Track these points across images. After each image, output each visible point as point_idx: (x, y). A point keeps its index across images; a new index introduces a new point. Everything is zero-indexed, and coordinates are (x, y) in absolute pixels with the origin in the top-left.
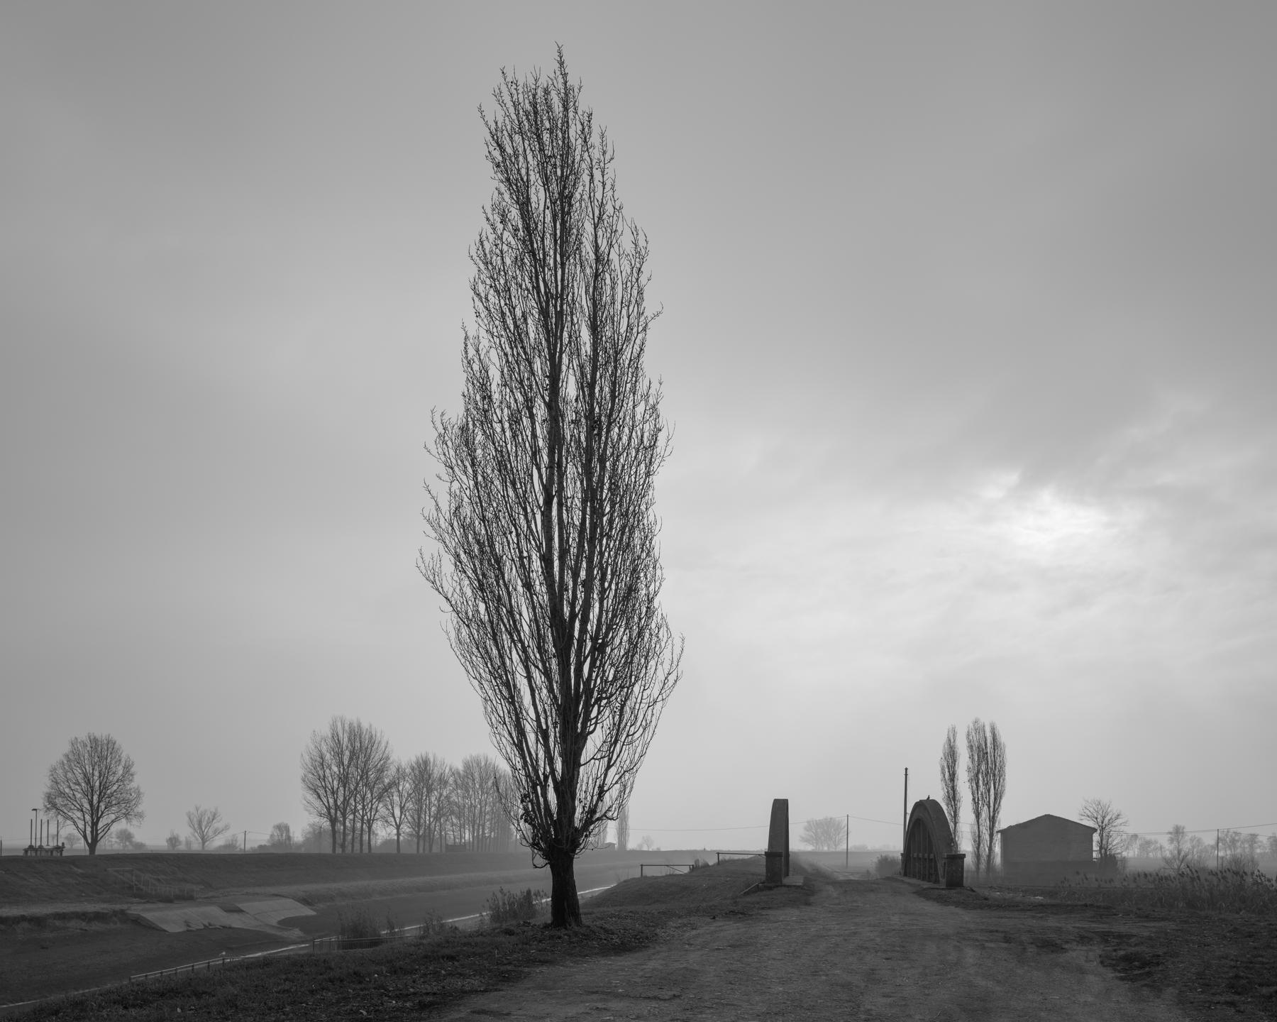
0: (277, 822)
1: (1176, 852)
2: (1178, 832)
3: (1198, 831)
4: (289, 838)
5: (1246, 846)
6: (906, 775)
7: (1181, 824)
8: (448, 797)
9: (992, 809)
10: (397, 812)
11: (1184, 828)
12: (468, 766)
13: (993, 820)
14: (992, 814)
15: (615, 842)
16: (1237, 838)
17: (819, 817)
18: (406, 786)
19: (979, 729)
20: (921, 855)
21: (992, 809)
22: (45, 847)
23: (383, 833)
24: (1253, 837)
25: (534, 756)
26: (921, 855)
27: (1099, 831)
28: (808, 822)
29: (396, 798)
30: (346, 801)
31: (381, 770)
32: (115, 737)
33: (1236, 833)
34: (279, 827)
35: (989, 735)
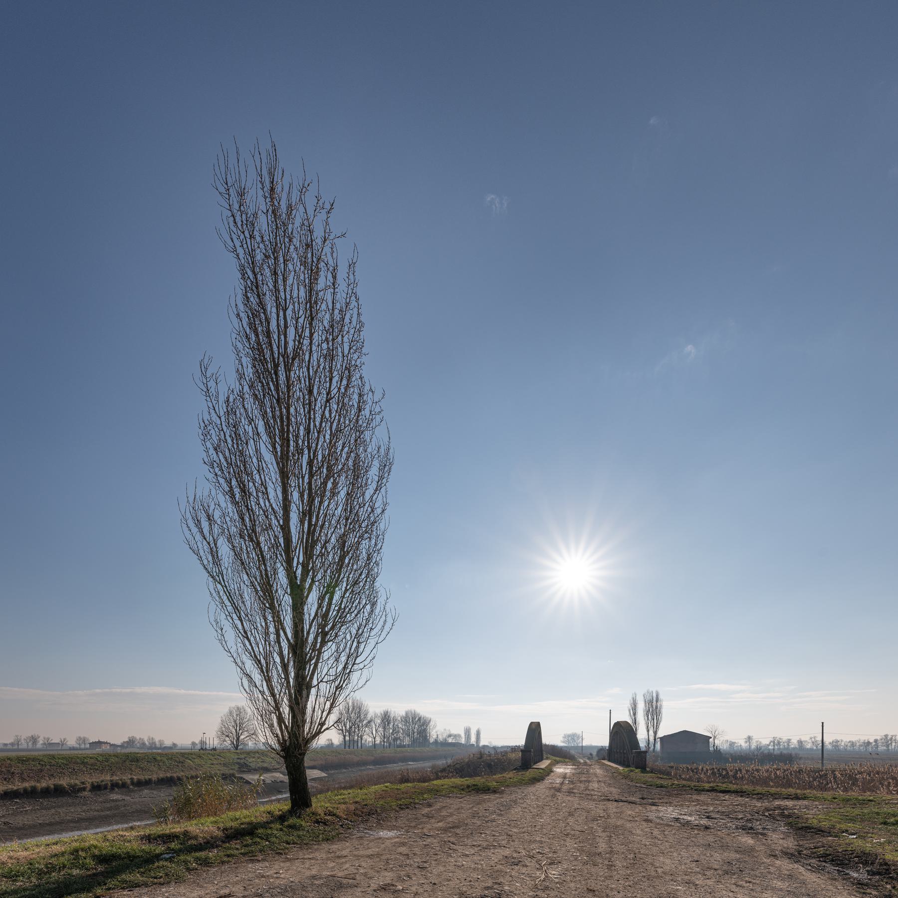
0: (328, 738)
1: (748, 747)
2: (749, 739)
3: (740, 739)
4: (332, 744)
5: (785, 744)
6: (610, 713)
7: (751, 735)
8: (397, 725)
9: (655, 729)
10: (374, 732)
11: (752, 736)
12: (407, 713)
13: (655, 733)
14: (655, 730)
15: (474, 743)
16: (781, 741)
17: (570, 732)
18: (378, 721)
19: (149, 737)
20: (618, 751)
21: (655, 729)
22: (208, 748)
23: (368, 739)
24: (789, 741)
25: (323, 719)
26: (618, 751)
27: (713, 738)
28: (565, 734)
29: (374, 726)
30: (351, 728)
31: (366, 714)
32: (85, 736)
33: (780, 739)
34: (328, 740)
35: (654, 695)
